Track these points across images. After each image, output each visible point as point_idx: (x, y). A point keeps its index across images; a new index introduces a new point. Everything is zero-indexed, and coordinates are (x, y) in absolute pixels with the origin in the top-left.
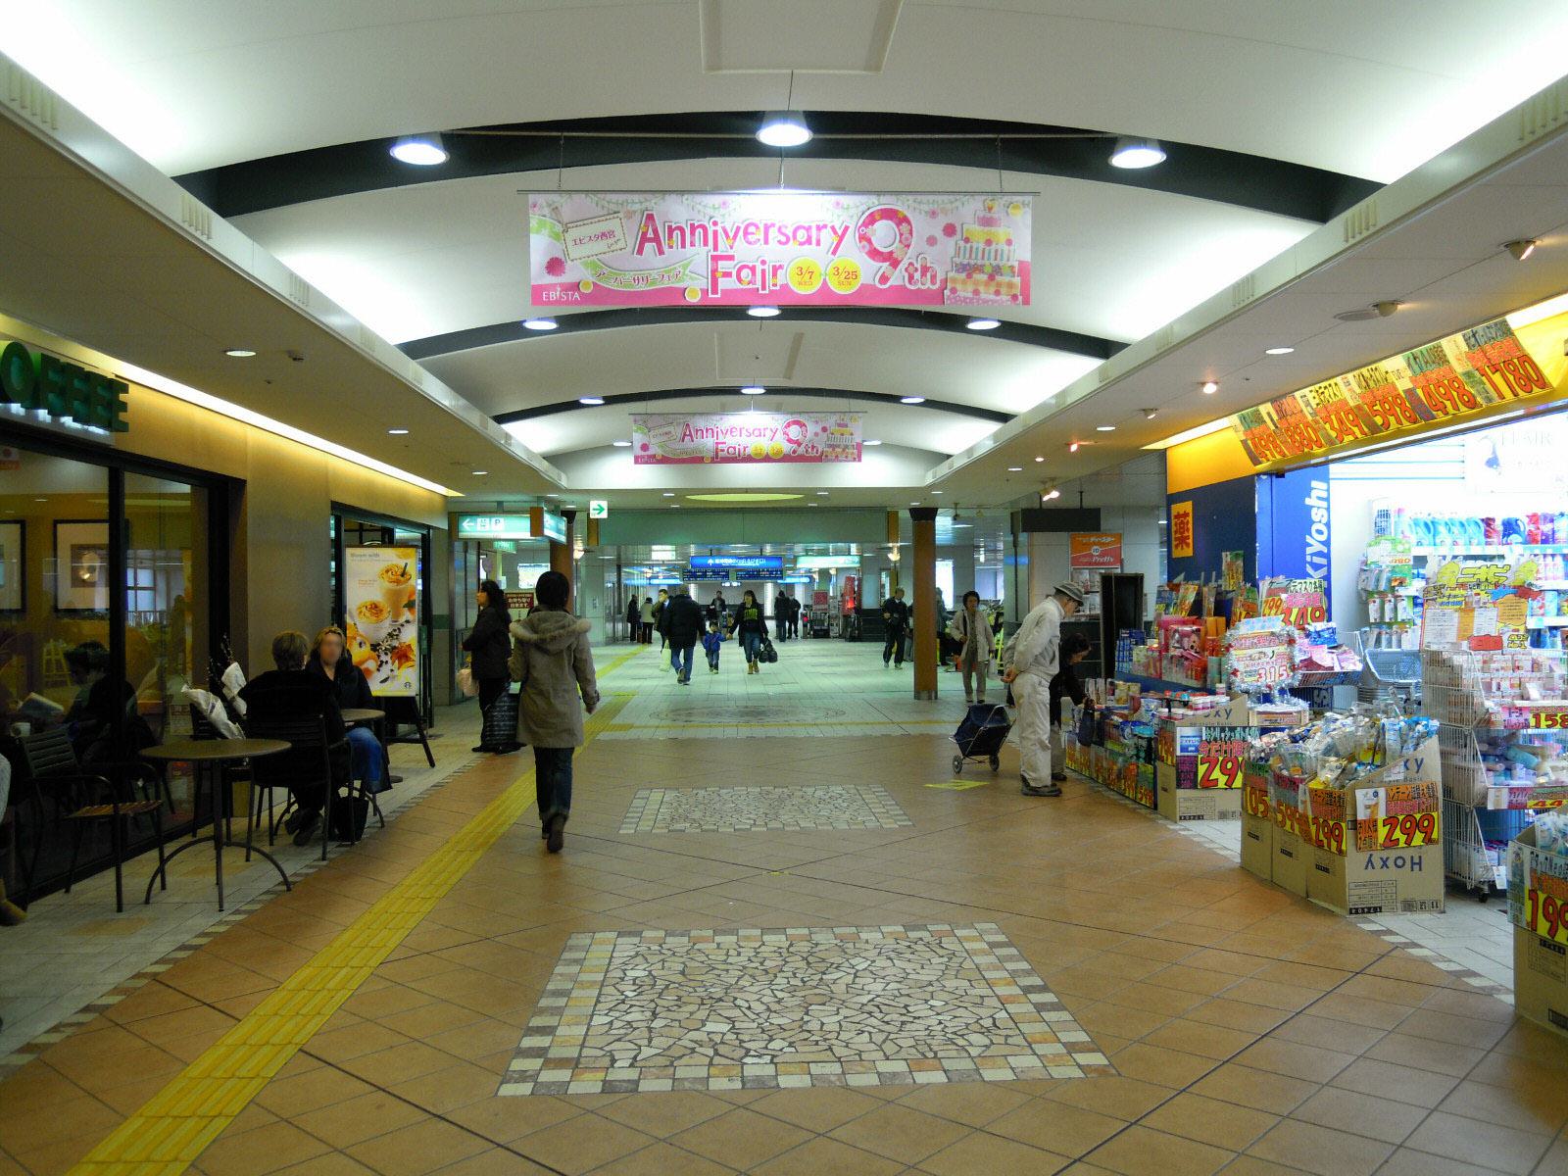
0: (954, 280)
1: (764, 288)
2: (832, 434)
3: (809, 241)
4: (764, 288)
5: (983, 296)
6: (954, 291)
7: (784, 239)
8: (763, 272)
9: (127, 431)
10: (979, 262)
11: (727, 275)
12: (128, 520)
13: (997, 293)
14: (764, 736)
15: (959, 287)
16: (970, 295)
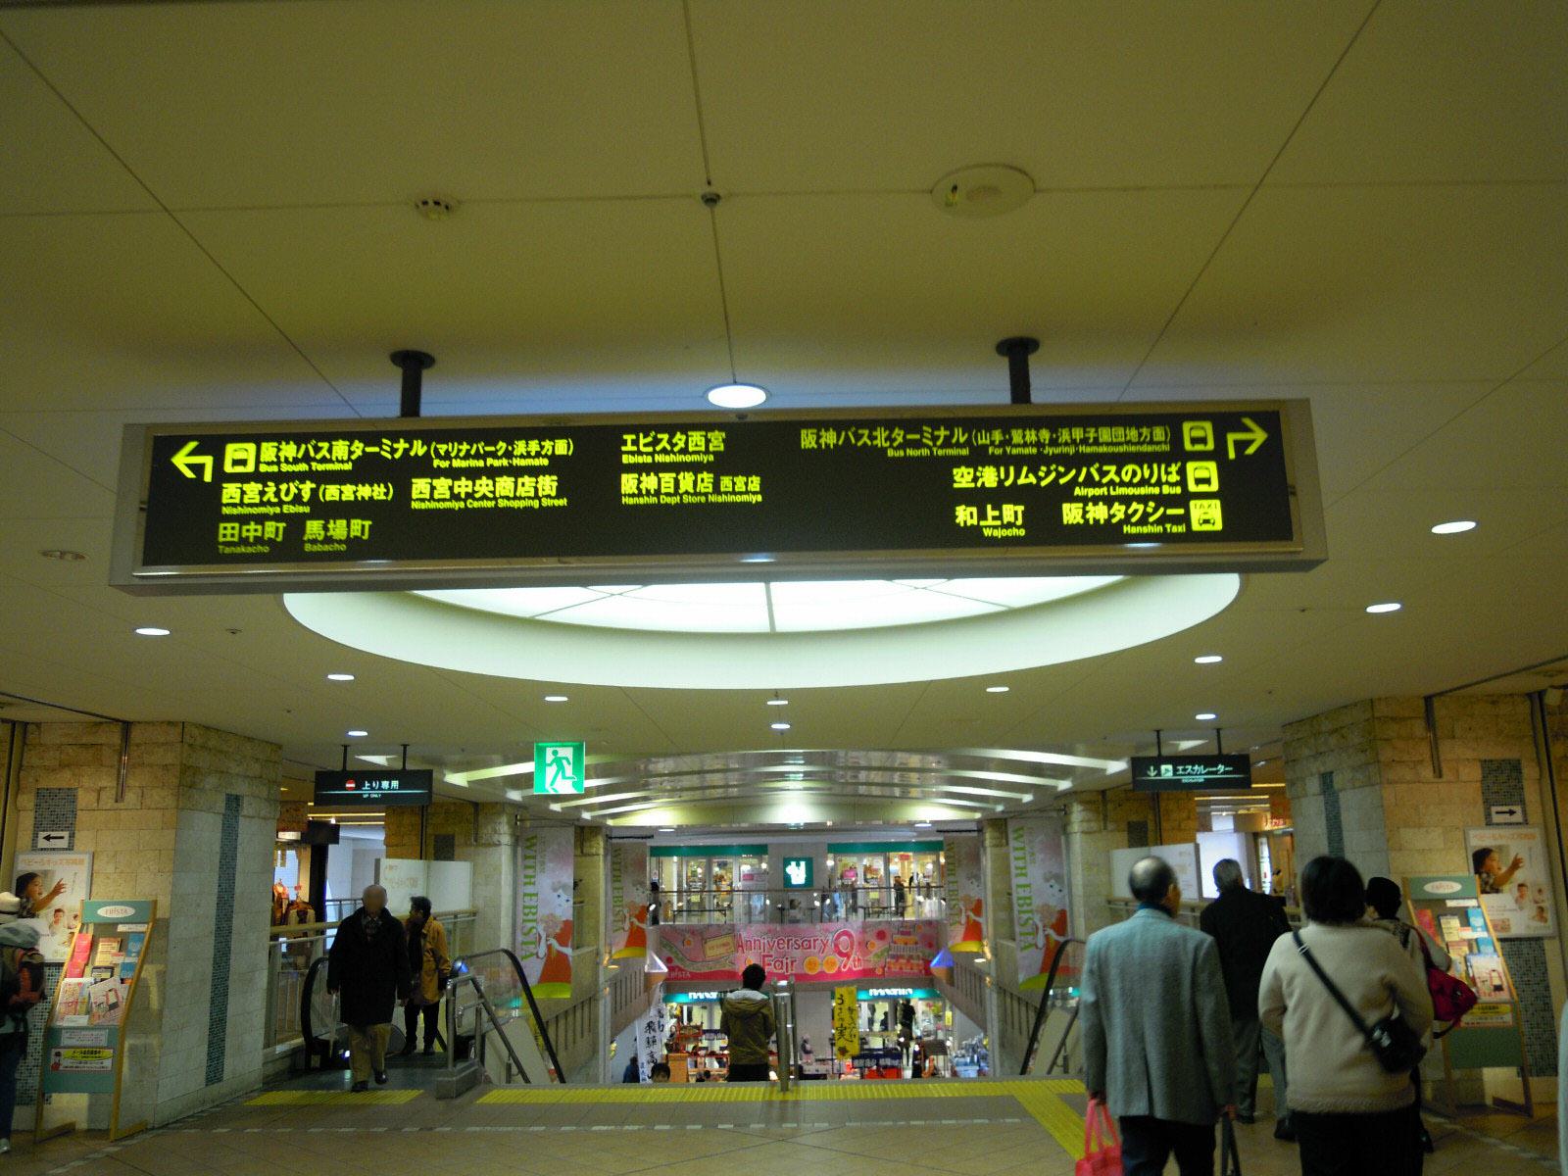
3: (810, 947)
5: (893, 970)
11: (769, 965)
16: (897, 970)
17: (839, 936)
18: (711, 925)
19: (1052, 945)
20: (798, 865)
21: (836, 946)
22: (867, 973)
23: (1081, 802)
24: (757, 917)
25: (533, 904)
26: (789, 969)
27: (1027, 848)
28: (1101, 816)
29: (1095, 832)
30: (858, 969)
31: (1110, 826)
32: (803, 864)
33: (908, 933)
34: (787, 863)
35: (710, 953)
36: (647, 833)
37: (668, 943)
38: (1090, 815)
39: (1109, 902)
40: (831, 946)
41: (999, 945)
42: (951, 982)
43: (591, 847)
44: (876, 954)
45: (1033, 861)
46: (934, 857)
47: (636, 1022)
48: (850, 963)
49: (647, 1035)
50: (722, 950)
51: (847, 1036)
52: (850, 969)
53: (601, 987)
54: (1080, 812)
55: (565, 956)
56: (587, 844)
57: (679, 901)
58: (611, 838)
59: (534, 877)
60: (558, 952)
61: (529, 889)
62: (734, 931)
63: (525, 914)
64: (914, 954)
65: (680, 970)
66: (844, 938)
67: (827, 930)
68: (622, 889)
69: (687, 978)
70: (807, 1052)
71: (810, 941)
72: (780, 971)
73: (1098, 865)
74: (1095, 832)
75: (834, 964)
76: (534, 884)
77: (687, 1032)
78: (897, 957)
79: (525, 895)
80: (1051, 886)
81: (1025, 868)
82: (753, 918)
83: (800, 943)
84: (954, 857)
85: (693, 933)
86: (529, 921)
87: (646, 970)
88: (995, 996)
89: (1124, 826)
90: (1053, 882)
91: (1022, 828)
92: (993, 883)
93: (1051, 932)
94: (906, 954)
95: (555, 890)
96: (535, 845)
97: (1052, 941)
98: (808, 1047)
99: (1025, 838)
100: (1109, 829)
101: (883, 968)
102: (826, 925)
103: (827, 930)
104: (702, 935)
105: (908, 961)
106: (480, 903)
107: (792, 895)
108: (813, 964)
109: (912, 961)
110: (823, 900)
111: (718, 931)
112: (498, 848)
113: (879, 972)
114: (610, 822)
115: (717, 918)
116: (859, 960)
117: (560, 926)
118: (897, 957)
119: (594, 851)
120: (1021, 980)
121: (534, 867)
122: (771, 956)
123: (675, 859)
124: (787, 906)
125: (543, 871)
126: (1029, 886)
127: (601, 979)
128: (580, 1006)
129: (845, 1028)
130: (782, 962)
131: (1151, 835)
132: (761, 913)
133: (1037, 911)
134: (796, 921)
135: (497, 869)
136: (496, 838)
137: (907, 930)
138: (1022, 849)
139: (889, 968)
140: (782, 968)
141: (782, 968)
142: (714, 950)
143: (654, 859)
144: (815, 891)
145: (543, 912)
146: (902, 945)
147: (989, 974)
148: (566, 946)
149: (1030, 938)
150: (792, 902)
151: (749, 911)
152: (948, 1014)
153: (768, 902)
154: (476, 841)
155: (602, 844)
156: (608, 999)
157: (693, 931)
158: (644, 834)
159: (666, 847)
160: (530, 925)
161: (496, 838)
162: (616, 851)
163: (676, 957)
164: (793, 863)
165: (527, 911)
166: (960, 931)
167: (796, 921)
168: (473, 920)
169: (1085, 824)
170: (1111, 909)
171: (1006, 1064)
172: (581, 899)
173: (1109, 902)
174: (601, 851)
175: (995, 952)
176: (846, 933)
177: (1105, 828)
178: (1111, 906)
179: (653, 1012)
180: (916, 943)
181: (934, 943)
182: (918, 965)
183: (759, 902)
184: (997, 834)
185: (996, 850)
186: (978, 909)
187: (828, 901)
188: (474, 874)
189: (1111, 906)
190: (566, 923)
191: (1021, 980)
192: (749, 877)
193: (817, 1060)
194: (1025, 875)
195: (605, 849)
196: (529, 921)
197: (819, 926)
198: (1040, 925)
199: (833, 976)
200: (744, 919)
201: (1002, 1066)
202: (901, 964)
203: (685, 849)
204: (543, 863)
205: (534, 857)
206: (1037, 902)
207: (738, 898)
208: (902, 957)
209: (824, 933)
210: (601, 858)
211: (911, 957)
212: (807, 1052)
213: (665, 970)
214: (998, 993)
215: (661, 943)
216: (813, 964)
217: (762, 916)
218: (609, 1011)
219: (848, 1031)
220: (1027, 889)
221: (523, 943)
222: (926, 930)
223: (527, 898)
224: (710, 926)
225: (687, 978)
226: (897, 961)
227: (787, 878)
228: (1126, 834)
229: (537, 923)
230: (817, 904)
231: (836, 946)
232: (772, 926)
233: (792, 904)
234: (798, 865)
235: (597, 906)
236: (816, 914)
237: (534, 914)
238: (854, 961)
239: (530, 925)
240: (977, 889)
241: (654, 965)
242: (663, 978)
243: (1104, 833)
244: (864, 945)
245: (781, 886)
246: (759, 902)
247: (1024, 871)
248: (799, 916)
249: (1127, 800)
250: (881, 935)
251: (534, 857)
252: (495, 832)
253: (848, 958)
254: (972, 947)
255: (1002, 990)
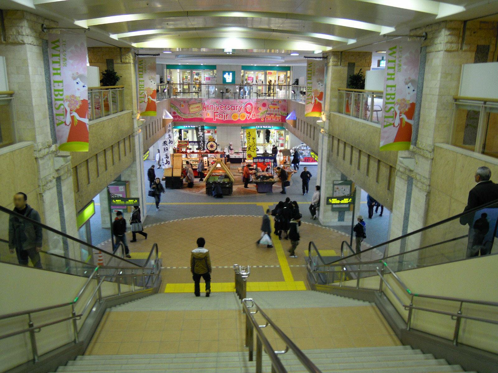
0: (267, 116)
1: (224, 119)
2: (270, 108)
3: (234, 109)
4: (224, 119)
5: (273, 120)
6: (267, 119)
7: (229, 109)
8: (224, 116)
9: (301, 217)
10: (272, 113)
11: (217, 116)
12: (294, 201)
13: (276, 119)
14: (243, 362)
15: (268, 118)
16: (270, 119)
17: (246, 106)
18: (192, 99)
19: (403, 125)
20: (229, 74)
21: (245, 109)
22: (258, 120)
23: (449, 29)
24: (212, 96)
25: (61, 88)
26: (225, 118)
27: (397, 61)
28: (461, 39)
29: (454, 51)
30: (254, 118)
31: (465, 48)
32: (231, 74)
33: (276, 105)
34: (224, 73)
35: (192, 110)
36: (156, 53)
37: (173, 105)
38: (454, 39)
39: (456, 100)
40: (243, 109)
41: (332, 116)
42: (295, 126)
43: (126, 59)
44: (262, 113)
45: (399, 71)
46: (285, 73)
47: (159, 141)
48: (251, 116)
49: (164, 147)
50: (197, 109)
51: (252, 149)
52: (251, 119)
53: (136, 130)
54: (447, 36)
55: (84, 124)
56: (123, 57)
57: (180, 88)
58: (138, 55)
59: (59, 69)
60: (79, 121)
61: (141, 79)
62: (202, 101)
63: (140, 88)
64: (277, 113)
65: (179, 117)
66: (249, 106)
67: (242, 102)
68: (312, 83)
69: (182, 121)
70: (231, 150)
71: (234, 107)
72: (222, 119)
73: (451, 74)
74: (454, 51)
75: (244, 116)
76: (60, 74)
77: (182, 144)
78: (270, 114)
79: (140, 81)
80: (409, 87)
81: (394, 74)
82: (210, 96)
83: (230, 107)
84: (311, 71)
85: (184, 102)
86: (142, 90)
87: (163, 118)
88: (326, 139)
89: (474, 48)
90: (410, 85)
91: (395, 48)
92: (331, 84)
93: (404, 116)
94: (274, 113)
95: (407, 83)
96: (58, 46)
97: (404, 122)
98: (232, 147)
99: (397, 55)
100: (464, 49)
101: (264, 118)
102: (242, 100)
103: (242, 102)
104: (188, 103)
105: (275, 116)
106: (15, 88)
107: (227, 87)
108: (236, 116)
109: (276, 116)
110: (240, 89)
111: (195, 102)
112: (23, 46)
113: (262, 120)
114: (135, 45)
115: (195, 96)
116: (254, 115)
117: (80, 103)
118: (270, 114)
119: (127, 61)
120: (381, 146)
121: (59, 62)
122: (218, 112)
123: (178, 70)
124: (225, 91)
125: (65, 65)
126: (395, 86)
127: (136, 126)
128: (123, 141)
129: (251, 146)
130: (222, 115)
131: (490, 55)
132: (213, 94)
133: (397, 103)
134: (228, 98)
135: (25, 61)
136: (20, 38)
137: (275, 103)
138: (394, 61)
139: (267, 119)
140: (222, 118)
141: (222, 118)
142: (194, 110)
143: (168, 70)
144: (237, 85)
145: (146, 87)
146: (273, 109)
147: (323, 128)
148: (154, 99)
149: (391, 120)
150: (227, 89)
151: (208, 93)
152: (288, 137)
153: (216, 89)
154: (5, 40)
155: (132, 57)
156: (141, 135)
157: (184, 101)
158: (155, 53)
159: (173, 65)
160: (142, 91)
161: (20, 38)
162: (140, 62)
163: (178, 112)
164: (227, 73)
165: (141, 87)
166: (311, 107)
167: (228, 98)
168: (11, 100)
169: (449, 45)
170: (456, 104)
171: (329, 170)
172: (123, 86)
173: (456, 100)
174: (132, 61)
175: (329, 118)
176: (249, 104)
177: (461, 49)
178: (457, 103)
179: (167, 136)
180: (278, 109)
181: (286, 109)
182: (279, 118)
183: (212, 89)
184: (335, 60)
185: (335, 68)
186: (321, 96)
187: (242, 90)
188: (7, 66)
189: (457, 103)
190: (84, 101)
191: (381, 146)
192: (209, 79)
193: (235, 153)
194: (393, 79)
195: (134, 60)
196: (142, 90)
197: (238, 101)
198: (398, 112)
199: (243, 121)
200: (206, 97)
201: (327, 170)
202: (272, 117)
203: (181, 66)
204: (65, 60)
205: (59, 56)
206: (398, 98)
207: (203, 87)
208: (272, 114)
209: (240, 103)
210: (132, 65)
211: (276, 114)
212: (231, 150)
213: (172, 118)
214: (329, 137)
215: (171, 105)
216: (236, 116)
217: (214, 95)
218: (141, 140)
219: (252, 147)
220: (393, 89)
221: (140, 98)
222: (282, 103)
223: (140, 82)
224: (192, 99)
225: (182, 121)
226: (270, 116)
227: (224, 79)
228: (474, 54)
229: (64, 102)
230: (238, 91)
231: (245, 109)
232: (218, 100)
233: (227, 91)
234: (229, 74)
235: (131, 89)
236: (237, 95)
237: (143, 88)
238: (252, 115)
239: (142, 91)
240: (321, 87)
241: (166, 115)
242: (172, 121)
243: (460, 52)
244: (257, 109)
245: (222, 83)
246: (212, 89)
247: (393, 77)
248: (230, 96)
249: (480, 29)
250: (264, 105)
251: (59, 56)
252: (19, 33)
253: (250, 114)
254: (316, 114)
255: (332, 137)
